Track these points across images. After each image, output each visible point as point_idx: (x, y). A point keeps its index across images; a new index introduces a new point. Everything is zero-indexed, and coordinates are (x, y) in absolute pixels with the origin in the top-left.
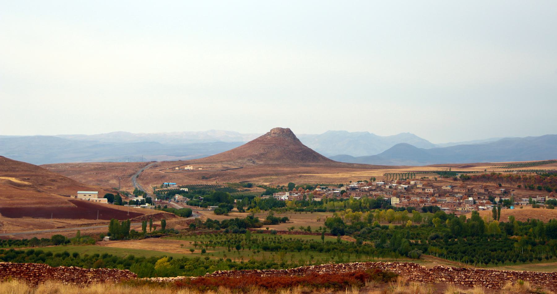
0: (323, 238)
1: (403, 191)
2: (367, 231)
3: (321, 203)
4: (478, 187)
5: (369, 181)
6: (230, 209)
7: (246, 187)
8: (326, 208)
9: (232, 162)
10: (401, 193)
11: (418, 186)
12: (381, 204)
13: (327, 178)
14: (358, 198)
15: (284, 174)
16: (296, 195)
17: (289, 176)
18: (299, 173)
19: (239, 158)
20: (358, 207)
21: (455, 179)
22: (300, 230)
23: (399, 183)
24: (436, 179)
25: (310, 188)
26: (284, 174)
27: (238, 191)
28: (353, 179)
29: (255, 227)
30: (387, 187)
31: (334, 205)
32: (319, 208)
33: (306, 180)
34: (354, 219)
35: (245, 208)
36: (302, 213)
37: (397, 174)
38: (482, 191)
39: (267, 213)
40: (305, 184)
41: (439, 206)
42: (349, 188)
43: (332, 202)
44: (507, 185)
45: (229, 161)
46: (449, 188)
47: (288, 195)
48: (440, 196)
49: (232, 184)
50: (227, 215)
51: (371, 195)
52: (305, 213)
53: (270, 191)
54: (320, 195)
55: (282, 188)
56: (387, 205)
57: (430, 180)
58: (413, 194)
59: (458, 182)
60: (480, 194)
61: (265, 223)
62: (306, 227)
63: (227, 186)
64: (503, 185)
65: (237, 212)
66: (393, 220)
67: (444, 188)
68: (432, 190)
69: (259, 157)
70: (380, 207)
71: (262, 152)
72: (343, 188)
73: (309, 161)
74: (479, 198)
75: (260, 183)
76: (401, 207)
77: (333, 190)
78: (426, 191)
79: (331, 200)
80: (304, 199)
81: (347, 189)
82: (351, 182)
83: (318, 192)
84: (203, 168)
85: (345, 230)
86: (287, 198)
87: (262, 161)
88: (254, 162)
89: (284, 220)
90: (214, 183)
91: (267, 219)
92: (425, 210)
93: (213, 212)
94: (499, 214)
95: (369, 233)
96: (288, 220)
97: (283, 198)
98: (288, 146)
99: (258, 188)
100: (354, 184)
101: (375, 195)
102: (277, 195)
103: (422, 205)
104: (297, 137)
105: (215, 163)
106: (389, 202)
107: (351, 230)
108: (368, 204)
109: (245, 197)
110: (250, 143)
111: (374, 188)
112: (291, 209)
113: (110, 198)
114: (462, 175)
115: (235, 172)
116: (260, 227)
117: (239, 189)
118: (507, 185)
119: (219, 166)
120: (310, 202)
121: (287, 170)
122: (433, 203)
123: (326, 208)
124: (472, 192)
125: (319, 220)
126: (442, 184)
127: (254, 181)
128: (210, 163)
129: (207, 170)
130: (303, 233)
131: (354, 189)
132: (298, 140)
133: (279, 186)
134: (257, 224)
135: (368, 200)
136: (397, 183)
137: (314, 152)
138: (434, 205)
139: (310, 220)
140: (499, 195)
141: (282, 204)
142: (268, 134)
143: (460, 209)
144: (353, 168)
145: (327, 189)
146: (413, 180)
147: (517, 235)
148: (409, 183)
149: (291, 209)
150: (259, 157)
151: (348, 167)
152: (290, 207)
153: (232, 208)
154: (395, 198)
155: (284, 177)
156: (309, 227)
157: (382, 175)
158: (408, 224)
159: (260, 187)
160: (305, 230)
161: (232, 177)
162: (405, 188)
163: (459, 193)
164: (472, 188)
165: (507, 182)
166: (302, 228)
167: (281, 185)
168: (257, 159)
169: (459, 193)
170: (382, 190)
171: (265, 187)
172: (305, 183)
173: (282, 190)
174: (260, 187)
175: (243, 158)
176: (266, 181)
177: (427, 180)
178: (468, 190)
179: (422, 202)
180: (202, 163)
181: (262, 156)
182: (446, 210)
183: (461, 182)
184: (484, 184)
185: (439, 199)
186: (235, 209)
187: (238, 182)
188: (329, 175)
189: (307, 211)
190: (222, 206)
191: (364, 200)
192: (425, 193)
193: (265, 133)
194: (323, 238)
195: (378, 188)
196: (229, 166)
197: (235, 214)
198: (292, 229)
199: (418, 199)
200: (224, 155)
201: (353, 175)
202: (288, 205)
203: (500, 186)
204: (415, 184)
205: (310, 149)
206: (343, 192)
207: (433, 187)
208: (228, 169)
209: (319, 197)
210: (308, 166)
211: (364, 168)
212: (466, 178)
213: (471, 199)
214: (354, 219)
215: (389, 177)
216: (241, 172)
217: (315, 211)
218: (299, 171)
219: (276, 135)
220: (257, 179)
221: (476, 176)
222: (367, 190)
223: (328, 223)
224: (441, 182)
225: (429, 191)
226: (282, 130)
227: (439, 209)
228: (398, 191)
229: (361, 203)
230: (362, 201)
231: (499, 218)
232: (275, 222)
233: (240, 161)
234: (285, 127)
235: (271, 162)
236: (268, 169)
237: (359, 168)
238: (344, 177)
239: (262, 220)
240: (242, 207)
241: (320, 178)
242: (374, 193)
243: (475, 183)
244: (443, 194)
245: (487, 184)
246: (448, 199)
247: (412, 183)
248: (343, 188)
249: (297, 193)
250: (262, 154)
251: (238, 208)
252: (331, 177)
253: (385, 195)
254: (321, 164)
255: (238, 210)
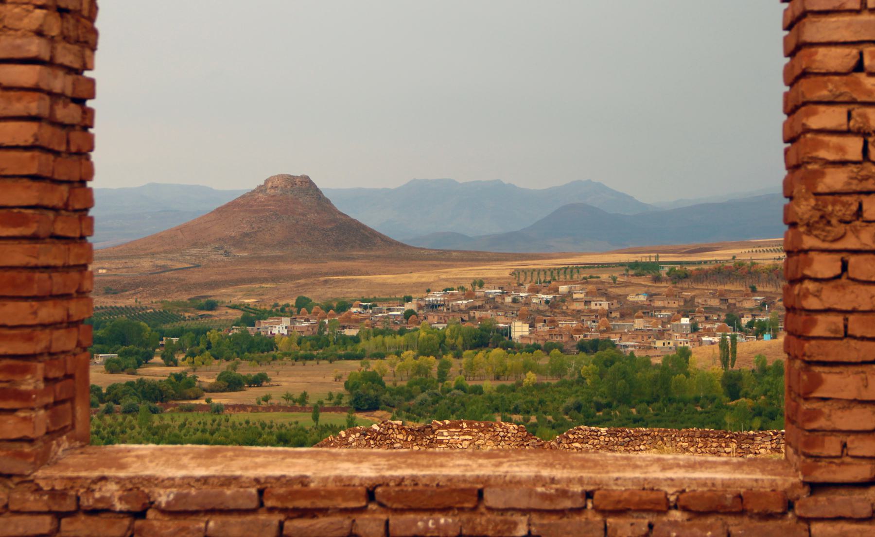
0: (316, 418)
1: (541, 308)
2: (430, 399)
3: (356, 340)
4: (705, 295)
5: (468, 287)
6: (145, 359)
7: (202, 308)
8: (363, 350)
9: (177, 255)
10: (538, 312)
11: (575, 296)
12: (487, 338)
13: (383, 285)
14: (440, 326)
15: (292, 277)
16: (306, 324)
17: (302, 281)
18: (326, 274)
19: (195, 245)
20: (438, 346)
21: (657, 279)
22: (283, 402)
23: (535, 291)
24: (614, 279)
25: (343, 307)
26: (292, 277)
27: (184, 319)
28: (433, 283)
29: (185, 399)
30: (508, 300)
31: (384, 344)
32: (349, 349)
33: (338, 290)
34: (418, 372)
35: (180, 357)
36: (309, 362)
37: (539, 271)
38: (715, 303)
39: (223, 366)
40: (336, 299)
41: (615, 338)
42: (423, 303)
43: (379, 337)
44: (769, 289)
45: (171, 252)
46: (642, 298)
47: (288, 324)
48: (623, 316)
49: (172, 304)
50: (133, 374)
51: (472, 319)
52: (314, 362)
53: (251, 317)
54: (357, 321)
55: (282, 310)
56: (501, 338)
57: (603, 283)
58: (565, 314)
59: (664, 284)
60: (710, 309)
61: (213, 389)
62: (297, 396)
63: (159, 308)
64: (759, 289)
65: (160, 365)
66: (504, 372)
67: (632, 298)
68: (605, 305)
69: (238, 243)
70: (486, 345)
71: (247, 230)
72: (408, 306)
73: (352, 247)
74: (707, 318)
75: (235, 300)
76: (532, 342)
77: (389, 310)
78: (593, 306)
79: (382, 333)
80: (320, 333)
81: (420, 307)
82: (428, 291)
83: (353, 317)
84: (109, 269)
85: (382, 398)
86: (285, 332)
87: (245, 249)
88: (227, 254)
89: (258, 381)
90: (130, 302)
91: (219, 379)
92: (582, 347)
93: (103, 368)
94: (734, 352)
95: (435, 402)
96: (268, 380)
97: (275, 331)
98: (304, 215)
99: (230, 311)
100: (437, 297)
101: (480, 319)
102: (263, 325)
103: (579, 337)
104: (326, 195)
105: (139, 257)
106: (507, 332)
107: (397, 397)
108: (460, 339)
109: (187, 331)
110: (220, 210)
111: (477, 304)
112: (285, 355)
113: (832, 332)
114: (671, 270)
115: (182, 276)
116: (197, 398)
117: (187, 315)
118: (769, 289)
119: (146, 264)
120: (331, 339)
121: (298, 268)
122: (602, 332)
123: (363, 350)
124: (693, 305)
125: (338, 378)
126: (628, 289)
127: (223, 295)
128: (122, 258)
129: (118, 272)
130: (286, 409)
131: (433, 306)
132: (328, 201)
133: (276, 305)
134: (189, 392)
135: (460, 330)
136: (530, 290)
137: (364, 227)
138: (606, 336)
139: (320, 379)
140: (751, 310)
141: (268, 345)
142: (261, 189)
143: (659, 344)
144: (448, 260)
145: (375, 309)
146: (565, 283)
147: (746, 395)
148: (556, 290)
149: (285, 355)
150: (238, 243)
151: (437, 259)
152: (285, 350)
153: (149, 356)
154: (520, 324)
155: (290, 285)
156: (304, 396)
157: (506, 274)
158: (526, 381)
159: (234, 307)
160: (294, 401)
161: (173, 288)
162: (547, 302)
163: (664, 308)
164: (693, 298)
165: (769, 281)
166: (288, 397)
167: (282, 303)
168: (234, 245)
169: (664, 308)
170: (496, 308)
171: (246, 308)
172: (335, 296)
173: (281, 312)
174: (234, 307)
175: (204, 245)
176: (248, 295)
177: (596, 283)
178: (686, 301)
179: (578, 331)
180: (108, 258)
181: (247, 239)
182: (630, 345)
183: (670, 285)
184: (720, 287)
185: (620, 323)
186: (157, 359)
187: (185, 297)
188: (389, 278)
189: (319, 358)
190: (126, 354)
191: (452, 331)
192: (592, 311)
193: (254, 187)
194: (316, 418)
195: (492, 303)
196: (169, 263)
197: (157, 372)
198: (266, 399)
199: (575, 324)
200: (159, 238)
201: (444, 276)
202: (280, 346)
203: (754, 290)
204: (570, 293)
205: (353, 220)
206: (408, 314)
207: (609, 297)
208: (165, 269)
209: (355, 327)
210: (348, 259)
211: (472, 260)
212: (679, 276)
213: (685, 321)
214: (418, 372)
215: (522, 277)
216: (196, 276)
217: (340, 358)
218: (325, 270)
219: (278, 192)
220: (229, 290)
221: (701, 270)
222: (462, 307)
223: (350, 385)
224: (626, 285)
225: (598, 307)
226: (291, 180)
227: (613, 345)
228: (532, 308)
229: (445, 337)
230: (448, 332)
231: (734, 360)
232: (233, 384)
233: (195, 251)
234: (297, 172)
235: (266, 253)
236: (258, 267)
237: (462, 260)
238: (423, 280)
239: (206, 379)
240: (172, 354)
241: (370, 284)
242: (478, 314)
243: (701, 286)
244: (629, 312)
245: (727, 287)
246: (639, 324)
247: (563, 289)
248: (408, 306)
249: (307, 320)
250: (246, 235)
251: (163, 357)
252: (393, 281)
253: (503, 319)
254: (379, 253)
255: (162, 361)
